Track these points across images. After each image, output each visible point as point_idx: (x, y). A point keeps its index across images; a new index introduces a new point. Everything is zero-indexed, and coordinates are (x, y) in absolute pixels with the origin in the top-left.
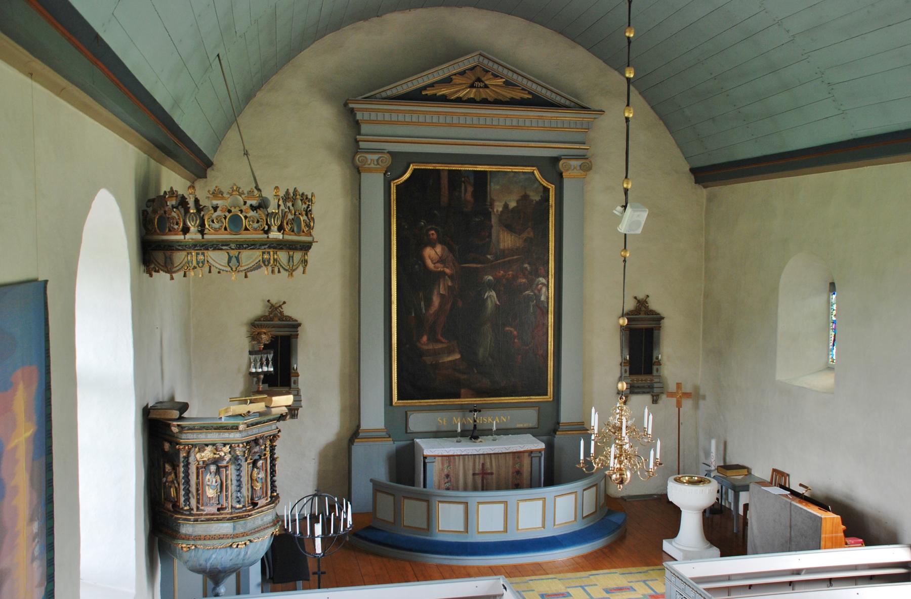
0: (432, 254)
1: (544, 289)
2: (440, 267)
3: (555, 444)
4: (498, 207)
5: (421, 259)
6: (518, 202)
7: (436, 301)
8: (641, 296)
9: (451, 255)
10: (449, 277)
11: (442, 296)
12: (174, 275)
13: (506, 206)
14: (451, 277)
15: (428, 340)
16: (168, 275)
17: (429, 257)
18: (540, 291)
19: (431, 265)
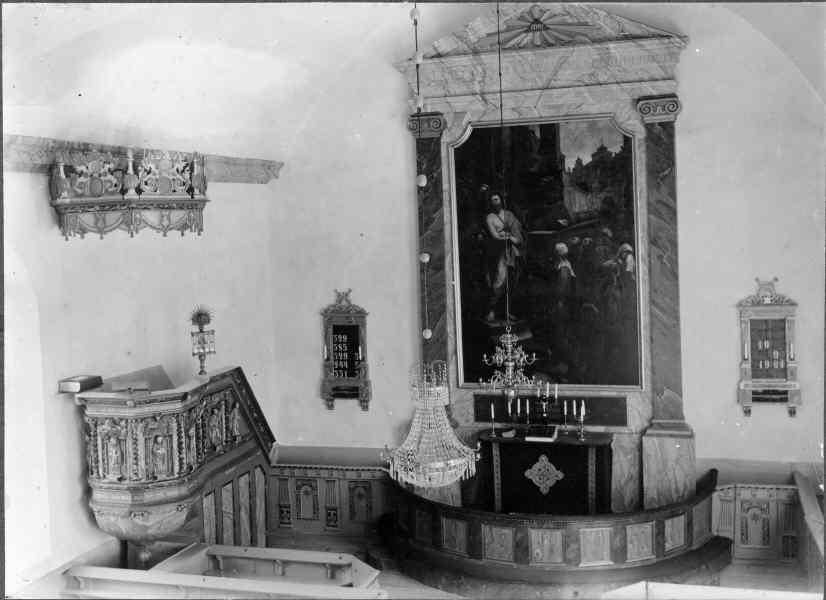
0: (496, 222)
1: (630, 258)
2: (505, 236)
3: (167, 372)
4: (570, 164)
5: (485, 227)
6: (593, 156)
7: (502, 271)
8: (343, 289)
9: (517, 221)
10: (515, 245)
11: (510, 269)
12: (104, 236)
13: (579, 162)
14: (518, 246)
15: (496, 317)
16: (99, 236)
17: (493, 224)
18: (624, 260)
19: (496, 234)
